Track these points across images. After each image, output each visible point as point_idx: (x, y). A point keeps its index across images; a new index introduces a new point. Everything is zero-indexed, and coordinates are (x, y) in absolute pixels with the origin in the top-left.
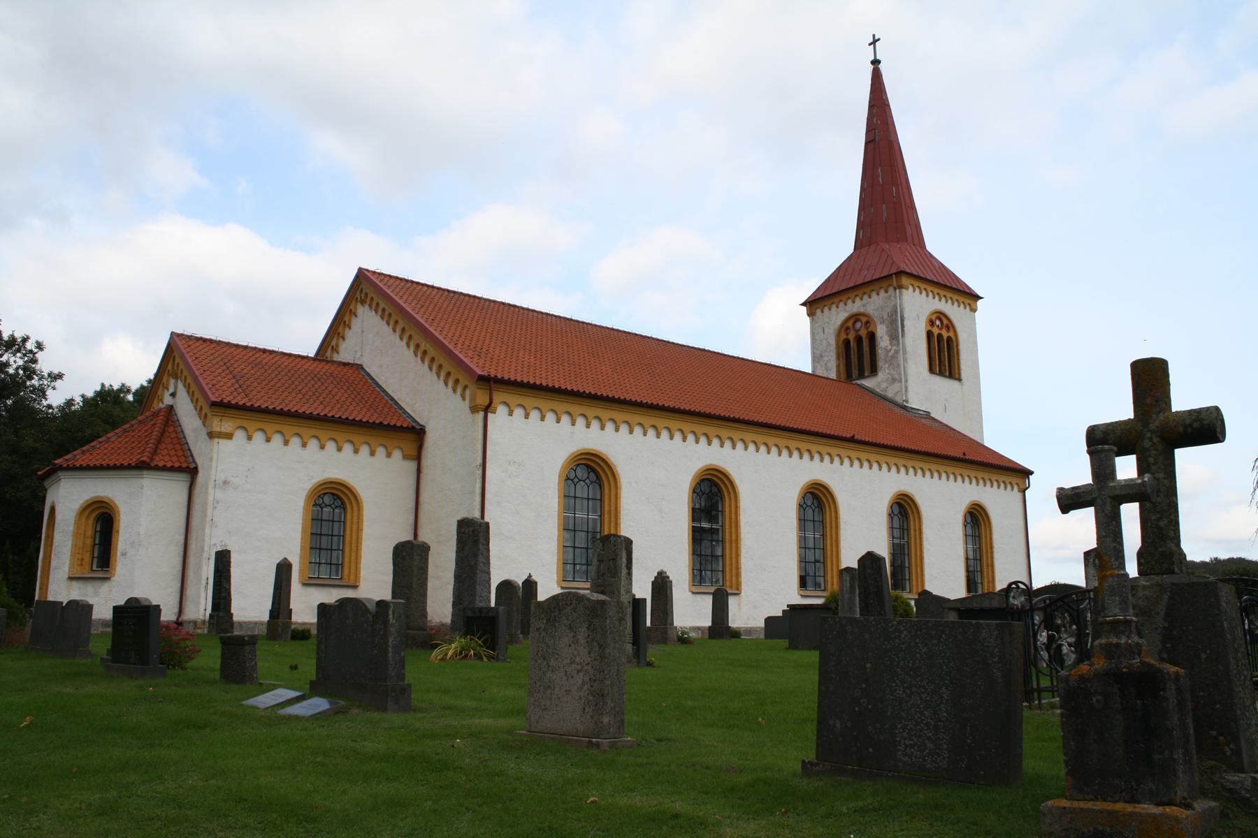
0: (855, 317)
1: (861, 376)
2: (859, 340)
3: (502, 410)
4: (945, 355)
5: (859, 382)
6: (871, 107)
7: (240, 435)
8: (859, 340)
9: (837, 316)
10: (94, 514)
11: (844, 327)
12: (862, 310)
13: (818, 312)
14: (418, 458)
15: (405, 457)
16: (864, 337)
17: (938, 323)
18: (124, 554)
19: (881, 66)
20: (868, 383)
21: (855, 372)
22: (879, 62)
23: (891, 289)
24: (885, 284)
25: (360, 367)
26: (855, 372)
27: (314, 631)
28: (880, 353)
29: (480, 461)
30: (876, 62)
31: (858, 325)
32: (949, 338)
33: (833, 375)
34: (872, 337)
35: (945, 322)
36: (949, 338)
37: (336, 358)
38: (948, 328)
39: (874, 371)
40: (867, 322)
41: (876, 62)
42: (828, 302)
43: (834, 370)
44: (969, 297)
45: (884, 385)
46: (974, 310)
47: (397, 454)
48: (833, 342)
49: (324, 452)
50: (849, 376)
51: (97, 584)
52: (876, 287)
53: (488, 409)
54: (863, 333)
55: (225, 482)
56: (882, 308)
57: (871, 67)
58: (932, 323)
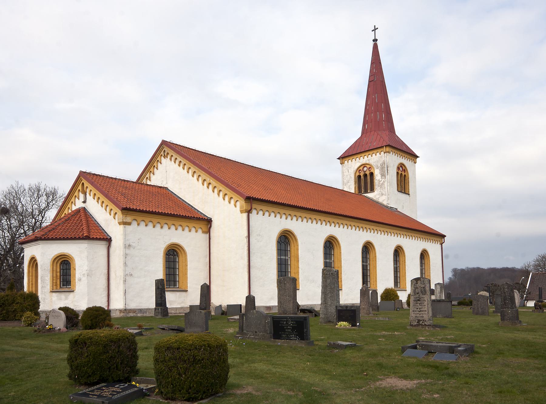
0: (364, 165)
1: (366, 192)
2: (365, 175)
3: (254, 212)
4: (403, 183)
5: (365, 195)
6: (372, 63)
7: (135, 223)
8: (365, 175)
9: (354, 164)
10: (58, 265)
11: (358, 170)
12: (367, 162)
13: (346, 162)
14: (209, 232)
15: (203, 232)
16: (368, 175)
17: (401, 169)
18: (80, 280)
19: (378, 42)
20: (370, 195)
21: (363, 190)
22: (377, 40)
23: (382, 153)
24: (379, 150)
25: (167, 188)
26: (363, 190)
27: (81, 315)
28: (376, 182)
29: (246, 234)
30: (375, 40)
31: (365, 169)
32: (405, 175)
33: (353, 191)
34: (372, 174)
35: (404, 168)
36: (405, 175)
37: (149, 183)
38: (405, 172)
39: (372, 190)
40: (370, 168)
41: (375, 40)
42: (351, 158)
43: (354, 189)
44: (414, 156)
45: (378, 197)
46: (415, 163)
47: (200, 231)
48: (353, 176)
49: (169, 231)
50: (360, 191)
51: (67, 294)
52: (375, 151)
53: (249, 212)
54: (368, 173)
55: (129, 245)
56: (378, 161)
57: (372, 43)
58: (398, 168)
